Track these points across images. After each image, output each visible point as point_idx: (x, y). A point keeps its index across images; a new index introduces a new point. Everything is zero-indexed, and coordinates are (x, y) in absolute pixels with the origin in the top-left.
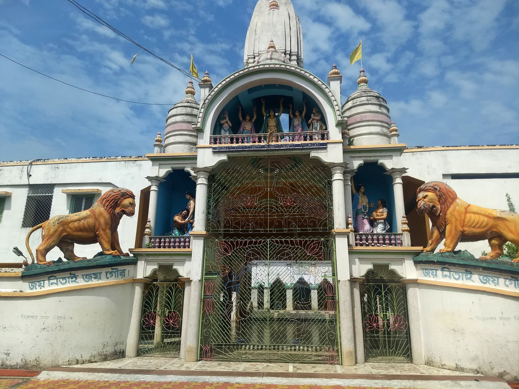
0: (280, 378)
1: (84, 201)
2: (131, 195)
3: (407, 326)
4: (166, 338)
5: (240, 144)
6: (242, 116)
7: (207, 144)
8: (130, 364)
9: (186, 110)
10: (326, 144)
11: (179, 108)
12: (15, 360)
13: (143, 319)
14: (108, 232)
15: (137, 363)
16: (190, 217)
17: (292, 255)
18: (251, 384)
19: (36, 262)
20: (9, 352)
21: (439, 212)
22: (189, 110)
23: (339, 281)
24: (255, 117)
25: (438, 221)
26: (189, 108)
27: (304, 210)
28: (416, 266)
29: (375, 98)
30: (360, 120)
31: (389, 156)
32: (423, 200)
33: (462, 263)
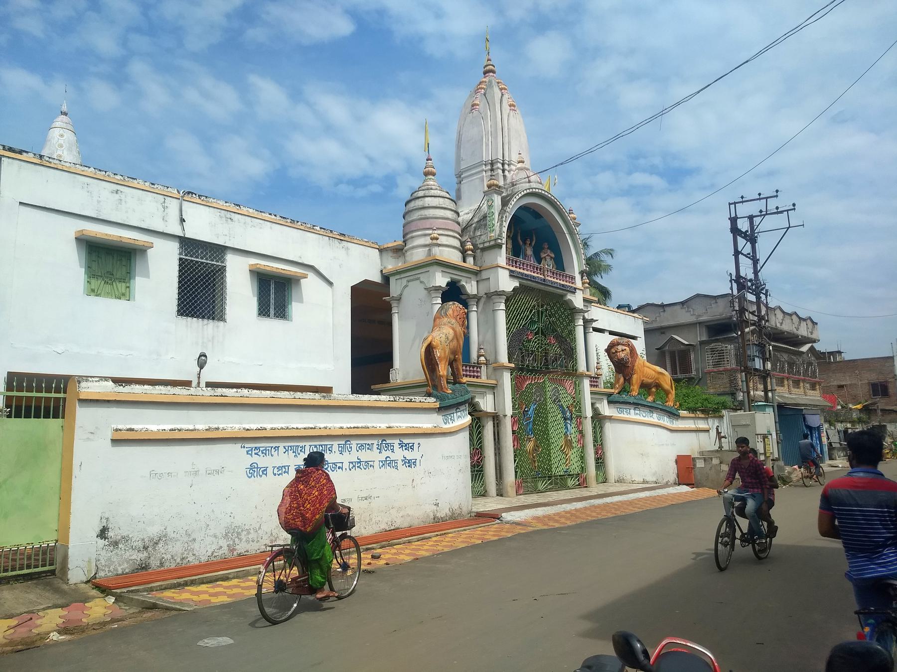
1: (272, 286)
20: (437, 502)
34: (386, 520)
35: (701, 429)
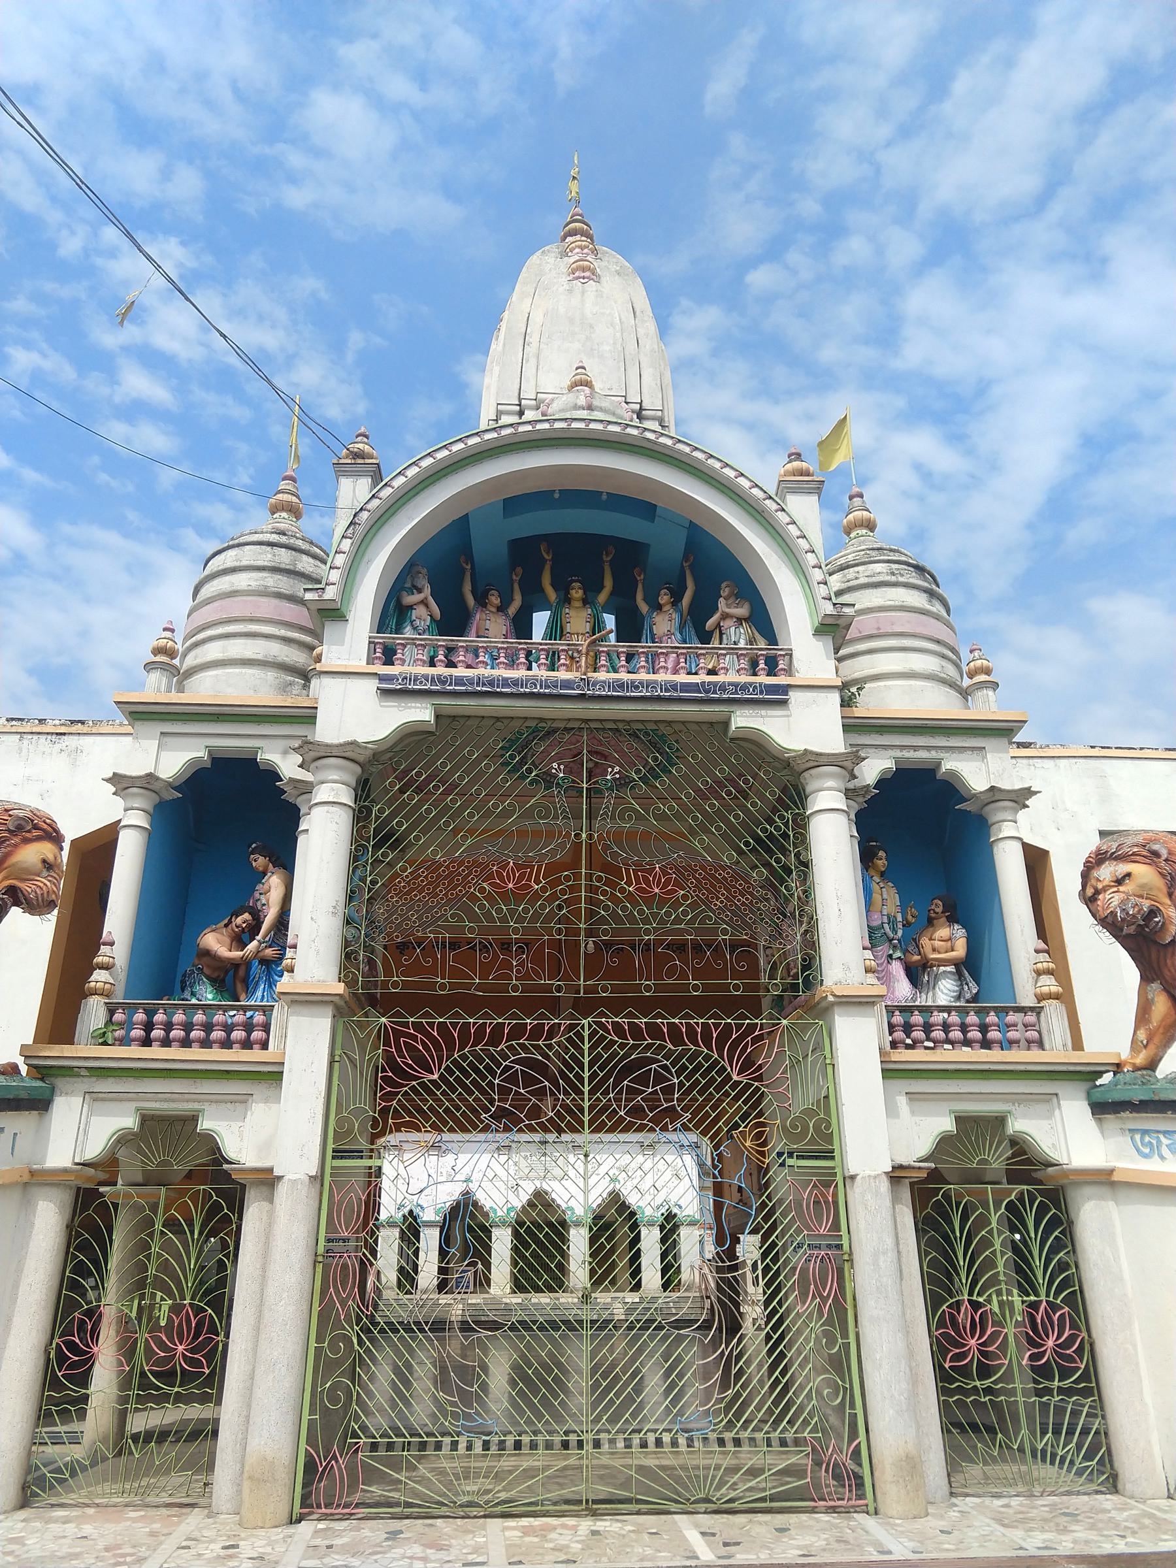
2: (49, 829)
3: (1087, 1347)
6: (473, 592)
9: (274, 555)
10: (785, 689)
11: (248, 547)
13: (56, 1340)
15: (24, 1545)
16: (264, 938)
17: (676, 1081)
22: (284, 557)
25: (1169, 962)
26: (283, 550)
27: (713, 912)
28: (1099, 1121)
29: (912, 569)
30: (875, 632)
31: (973, 749)
32: (1115, 889)
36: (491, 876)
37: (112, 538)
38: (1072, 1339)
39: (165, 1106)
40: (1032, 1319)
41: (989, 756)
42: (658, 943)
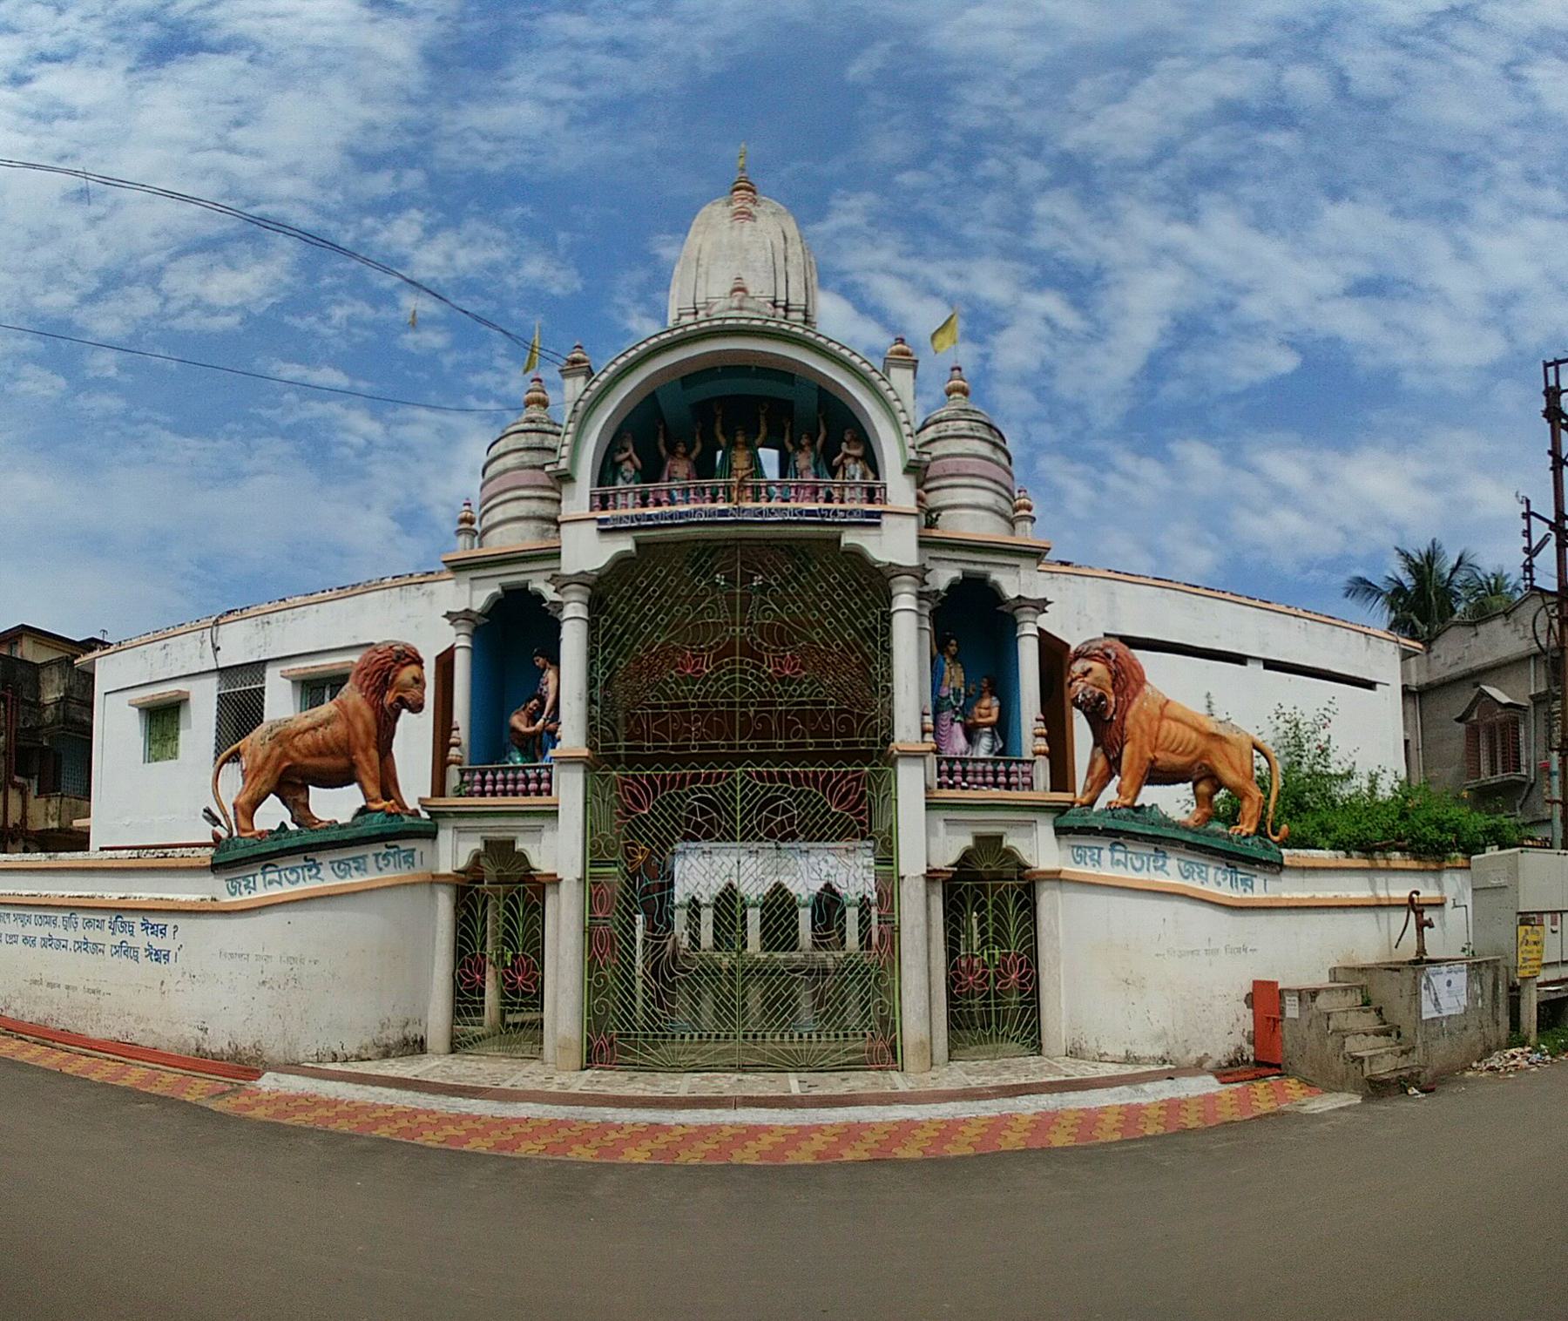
0: (777, 1110)
4: (511, 1012)
5: (666, 509)
6: (666, 446)
7: (586, 513)
8: (437, 1071)
10: (879, 514)
12: (218, 1043)
14: (374, 753)
18: (712, 1126)
19: (235, 833)
20: (205, 1026)
21: (1112, 710)
22: (535, 439)
23: (903, 878)
24: (699, 446)
28: (1059, 839)
31: (1011, 565)
33: (1150, 833)
34: (118, 1027)
35: (1394, 902)
36: (677, 666)
37: (423, 413)
38: (1026, 974)
39: (497, 835)
40: (1004, 963)
41: (1022, 572)
42: (788, 712)
